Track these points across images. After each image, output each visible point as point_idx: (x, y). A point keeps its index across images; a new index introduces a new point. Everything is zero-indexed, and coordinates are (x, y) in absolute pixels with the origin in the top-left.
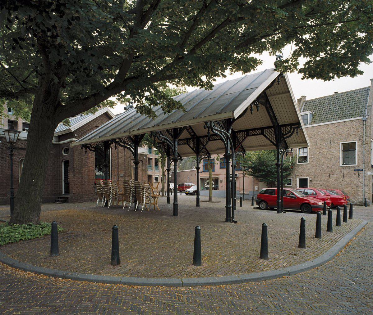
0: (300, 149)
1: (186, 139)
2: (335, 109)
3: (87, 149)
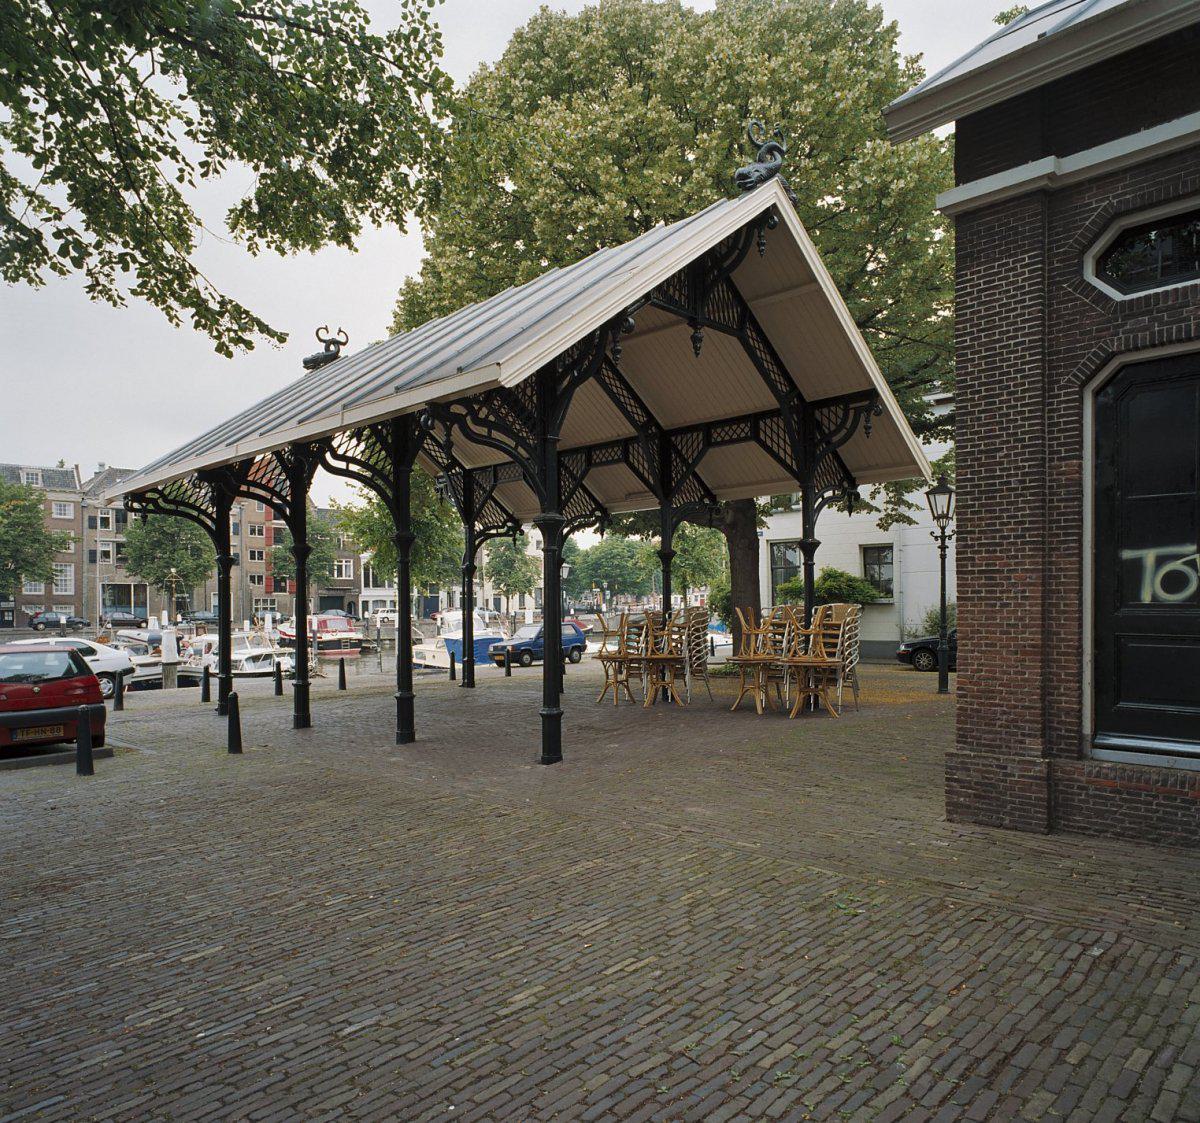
1: (617, 441)
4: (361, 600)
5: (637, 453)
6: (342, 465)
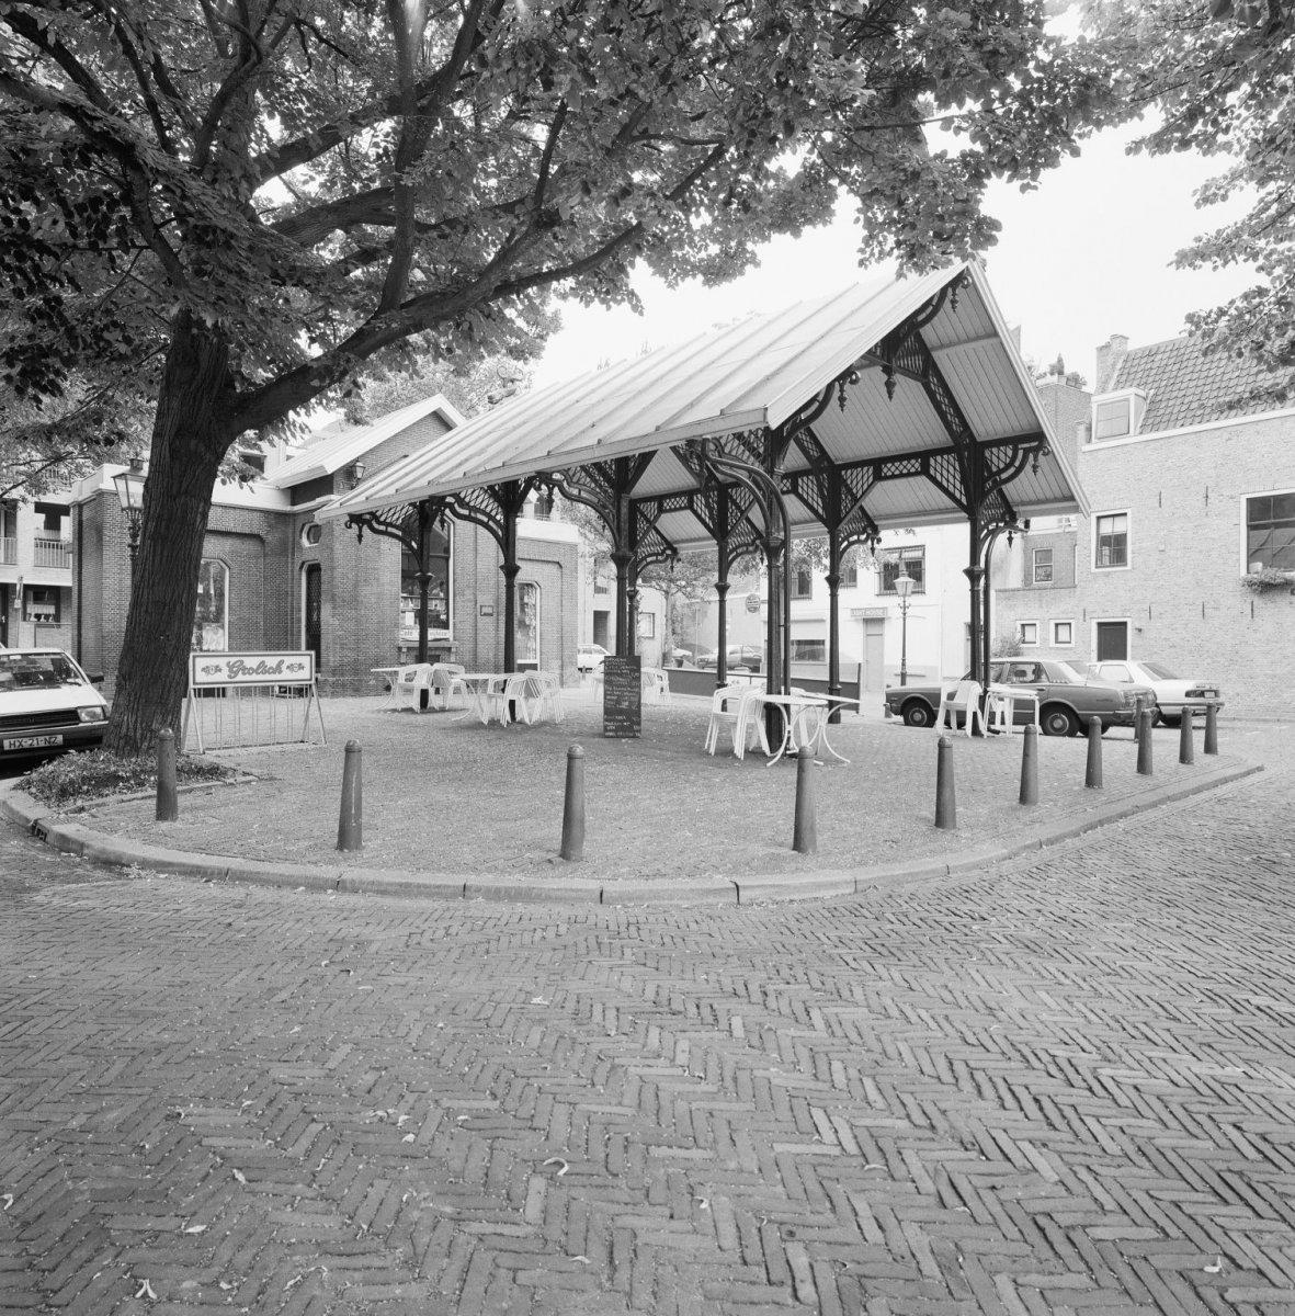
0: (1103, 521)
2: (1226, 377)
3: (556, 490)
5: (699, 501)
6: (382, 528)
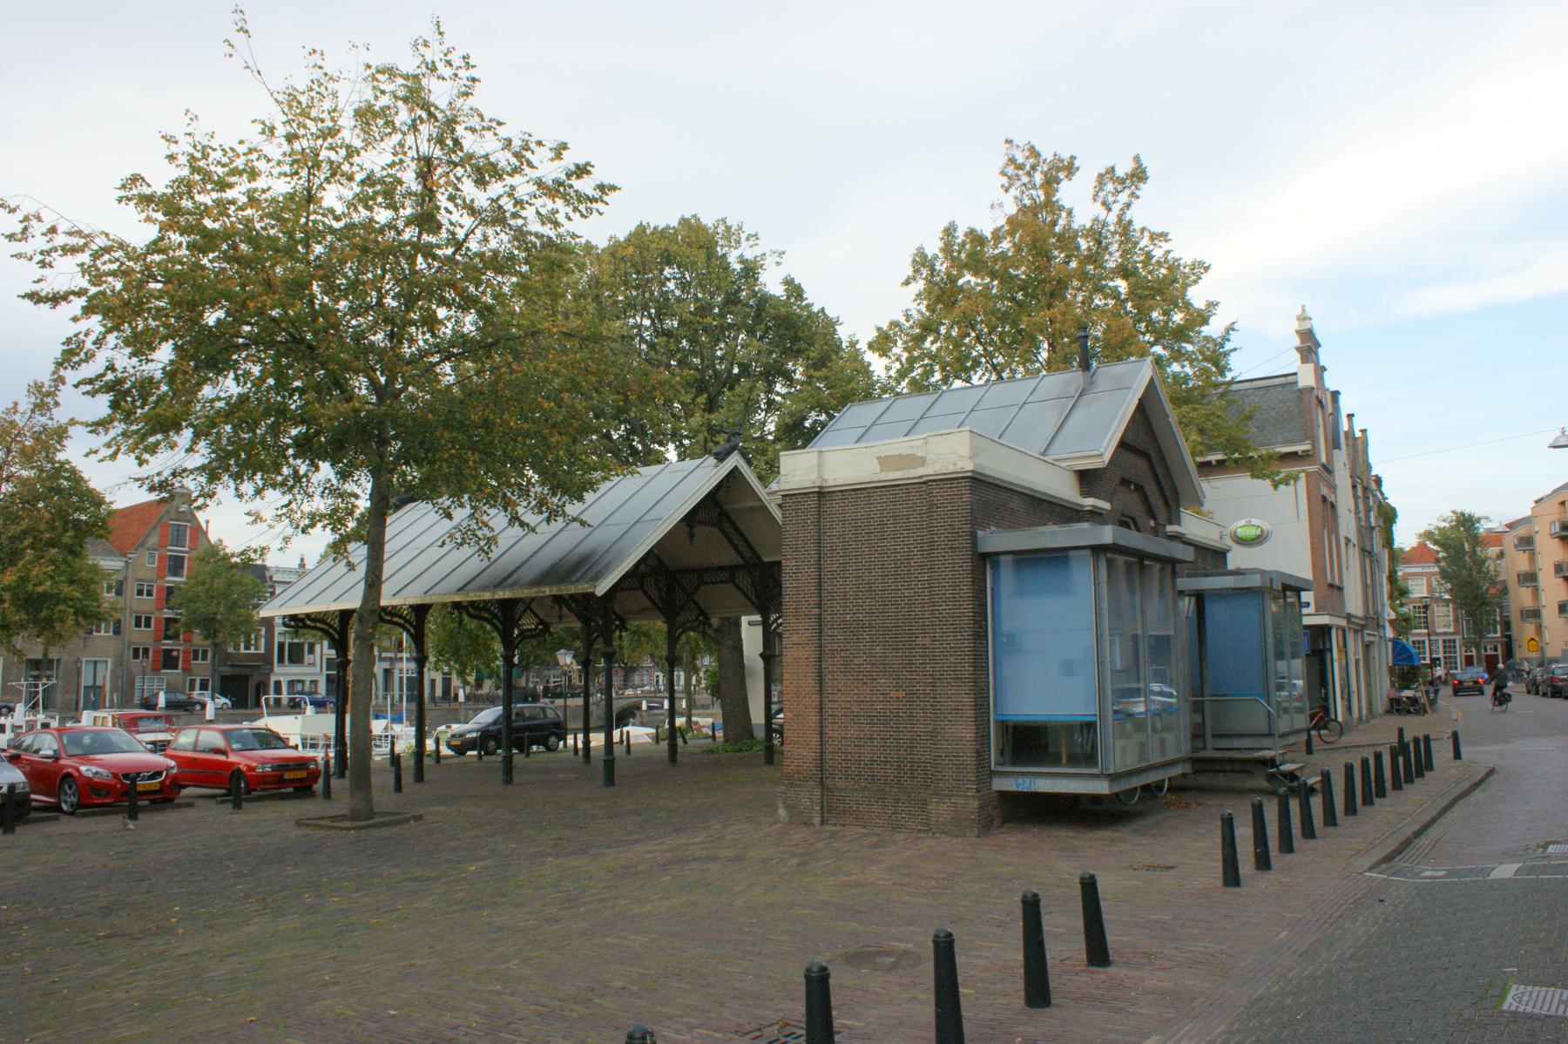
4: (273, 679)
